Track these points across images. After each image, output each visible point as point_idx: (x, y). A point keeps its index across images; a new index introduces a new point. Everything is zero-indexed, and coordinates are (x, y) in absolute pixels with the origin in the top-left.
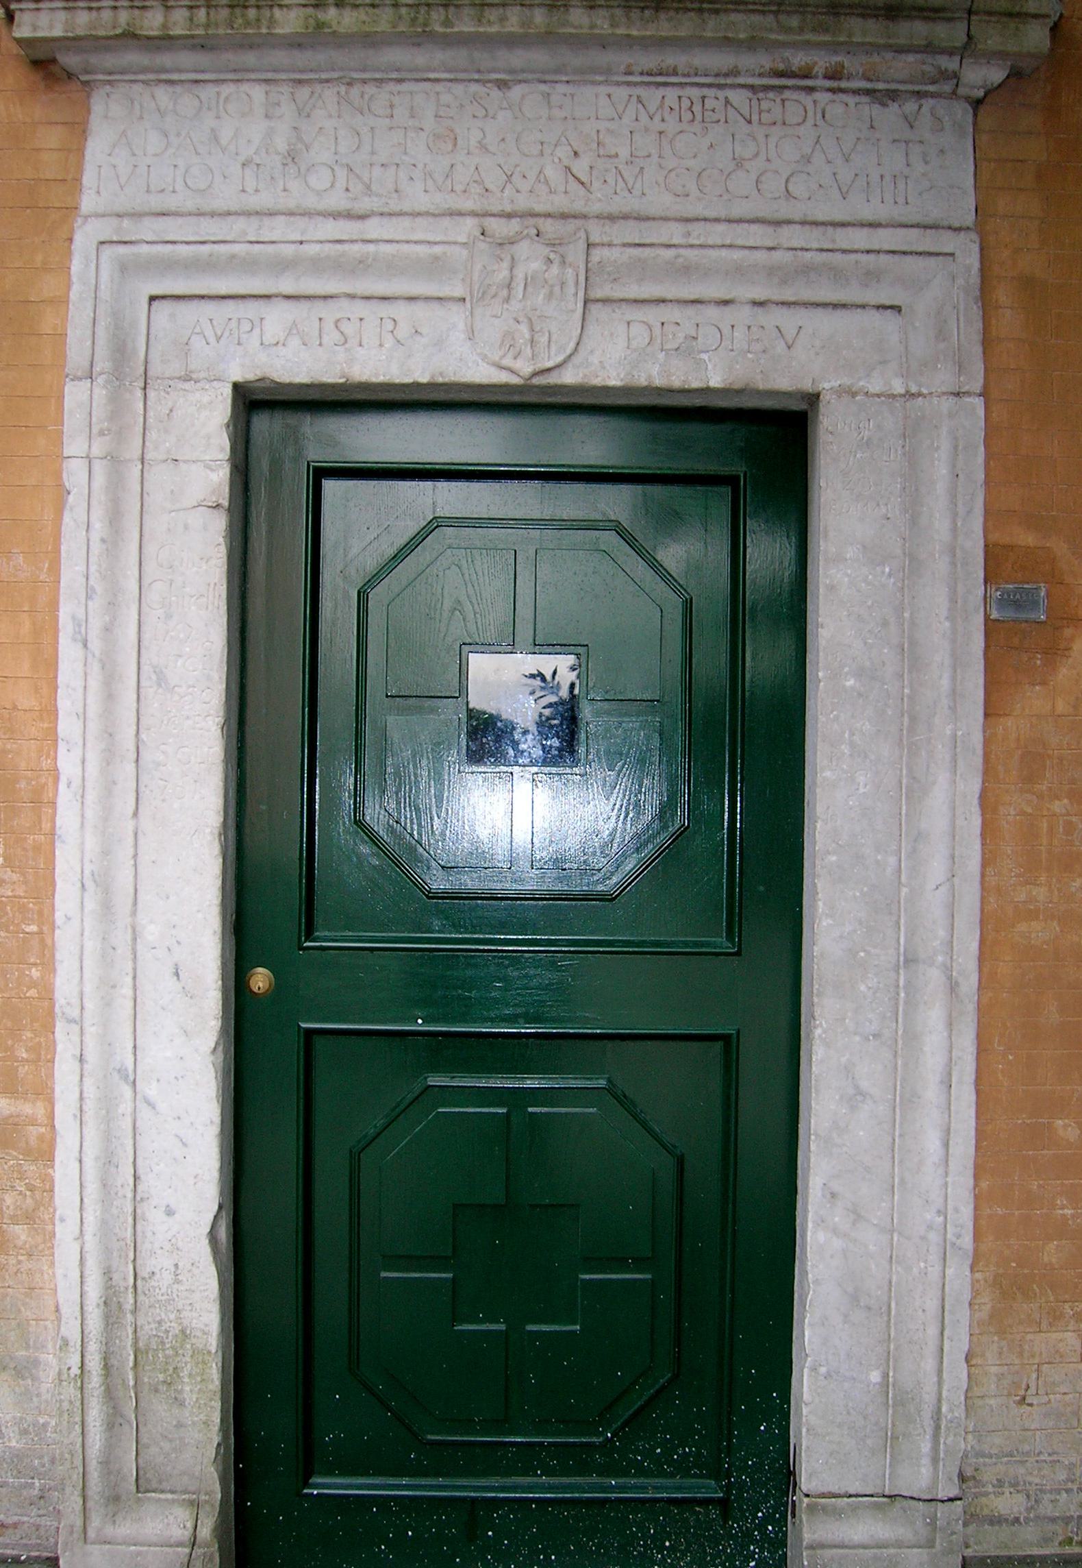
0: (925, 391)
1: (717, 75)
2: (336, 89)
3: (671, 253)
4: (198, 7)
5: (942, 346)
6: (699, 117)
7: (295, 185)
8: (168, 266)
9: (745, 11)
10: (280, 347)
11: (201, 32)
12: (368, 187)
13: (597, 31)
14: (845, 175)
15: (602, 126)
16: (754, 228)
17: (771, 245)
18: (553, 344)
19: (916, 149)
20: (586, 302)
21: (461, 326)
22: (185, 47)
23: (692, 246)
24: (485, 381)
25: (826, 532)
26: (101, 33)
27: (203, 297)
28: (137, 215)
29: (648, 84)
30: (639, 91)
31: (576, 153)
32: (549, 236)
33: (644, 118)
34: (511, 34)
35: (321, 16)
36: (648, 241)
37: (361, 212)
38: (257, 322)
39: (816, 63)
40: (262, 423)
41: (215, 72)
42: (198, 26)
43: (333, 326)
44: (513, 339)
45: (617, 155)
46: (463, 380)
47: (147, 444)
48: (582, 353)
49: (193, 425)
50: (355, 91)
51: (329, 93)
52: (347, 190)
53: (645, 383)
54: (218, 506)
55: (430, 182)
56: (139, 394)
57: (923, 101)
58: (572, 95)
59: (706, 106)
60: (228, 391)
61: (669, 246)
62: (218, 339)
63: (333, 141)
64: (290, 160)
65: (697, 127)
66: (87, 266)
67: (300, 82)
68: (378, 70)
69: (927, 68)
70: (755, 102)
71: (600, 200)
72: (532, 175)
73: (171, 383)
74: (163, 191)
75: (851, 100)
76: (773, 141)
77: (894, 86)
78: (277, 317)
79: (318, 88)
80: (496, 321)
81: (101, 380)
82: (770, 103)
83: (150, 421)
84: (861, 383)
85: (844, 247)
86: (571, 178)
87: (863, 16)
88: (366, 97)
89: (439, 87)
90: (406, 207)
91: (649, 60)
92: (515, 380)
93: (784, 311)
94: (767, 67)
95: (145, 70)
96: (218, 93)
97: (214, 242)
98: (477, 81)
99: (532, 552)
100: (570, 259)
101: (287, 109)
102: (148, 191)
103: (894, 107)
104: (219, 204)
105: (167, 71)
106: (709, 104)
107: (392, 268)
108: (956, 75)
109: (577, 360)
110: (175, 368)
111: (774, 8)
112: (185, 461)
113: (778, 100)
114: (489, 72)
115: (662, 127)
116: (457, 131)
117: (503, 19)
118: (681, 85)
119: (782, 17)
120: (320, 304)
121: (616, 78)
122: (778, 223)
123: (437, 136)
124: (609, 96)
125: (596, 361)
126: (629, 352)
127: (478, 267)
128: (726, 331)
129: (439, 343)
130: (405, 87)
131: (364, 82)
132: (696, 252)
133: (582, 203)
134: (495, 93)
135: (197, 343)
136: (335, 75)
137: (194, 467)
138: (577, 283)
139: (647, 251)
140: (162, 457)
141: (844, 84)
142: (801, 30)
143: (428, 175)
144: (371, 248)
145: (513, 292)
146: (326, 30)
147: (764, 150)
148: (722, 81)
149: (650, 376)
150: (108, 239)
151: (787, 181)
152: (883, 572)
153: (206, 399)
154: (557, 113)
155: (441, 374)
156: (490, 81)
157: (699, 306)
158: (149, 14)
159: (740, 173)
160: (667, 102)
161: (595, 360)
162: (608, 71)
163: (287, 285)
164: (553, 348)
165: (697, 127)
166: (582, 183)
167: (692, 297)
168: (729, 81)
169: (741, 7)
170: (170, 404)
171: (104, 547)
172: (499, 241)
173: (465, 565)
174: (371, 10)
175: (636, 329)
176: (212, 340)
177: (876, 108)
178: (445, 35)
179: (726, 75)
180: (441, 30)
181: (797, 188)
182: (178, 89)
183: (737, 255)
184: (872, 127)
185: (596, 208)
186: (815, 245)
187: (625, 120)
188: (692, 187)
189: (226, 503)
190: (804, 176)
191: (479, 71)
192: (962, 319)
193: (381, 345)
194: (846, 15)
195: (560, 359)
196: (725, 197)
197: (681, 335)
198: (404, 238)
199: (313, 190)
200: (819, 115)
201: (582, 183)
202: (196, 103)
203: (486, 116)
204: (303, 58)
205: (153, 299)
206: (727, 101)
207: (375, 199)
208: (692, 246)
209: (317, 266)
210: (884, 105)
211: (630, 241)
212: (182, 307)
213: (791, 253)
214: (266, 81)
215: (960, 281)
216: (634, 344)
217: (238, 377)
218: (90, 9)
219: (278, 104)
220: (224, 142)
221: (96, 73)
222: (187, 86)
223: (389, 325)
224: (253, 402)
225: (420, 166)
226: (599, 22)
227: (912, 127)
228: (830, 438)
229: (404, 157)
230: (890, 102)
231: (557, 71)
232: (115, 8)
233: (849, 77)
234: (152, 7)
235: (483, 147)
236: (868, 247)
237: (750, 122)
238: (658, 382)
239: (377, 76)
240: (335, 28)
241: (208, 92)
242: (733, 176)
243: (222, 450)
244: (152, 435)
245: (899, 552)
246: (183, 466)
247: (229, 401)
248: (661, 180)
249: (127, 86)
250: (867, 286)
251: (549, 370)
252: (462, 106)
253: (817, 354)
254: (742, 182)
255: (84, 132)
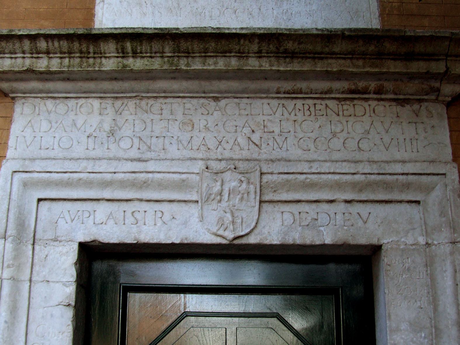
0: (435, 242)
1: (321, 93)
2: (134, 102)
3: (303, 177)
4: (65, 58)
5: (444, 219)
6: (313, 113)
7: (112, 146)
8: (48, 184)
9: (335, 58)
10: (103, 225)
11: (66, 69)
12: (150, 148)
13: (262, 68)
14: (387, 139)
15: (266, 118)
16: (344, 164)
17: (354, 172)
18: (244, 223)
19: (420, 127)
20: (261, 202)
21: (196, 215)
22: (59, 80)
23: (314, 173)
24: (209, 242)
25: (390, 316)
26: (16, 69)
27: (65, 200)
28: (33, 160)
29: (288, 98)
30: (283, 101)
31: (253, 131)
32: (241, 169)
33: (286, 114)
34: (220, 71)
35: (125, 62)
36: (292, 171)
37: (146, 159)
38: (92, 213)
39: (370, 85)
40: (99, 267)
41: (74, 93)
42: (64, 66)
43: (131, 215)
44: (223, 220)
45: (273, 132)
46: (198, 242)
47: (34, 272)
48: (259, 227)
49: (58, 263)
50: (144, 102)
51: (131, 104)
52: (139, 149)
53: (292, 243)
54: (69, 305)
55: (180, 145)
56: (30, 247)
57: (422, 104)
58: (251, 104)
59: (317, 108)
60: (76, 247)
61: (302, 173)
62: (72, 221)
63: (132, 126)
64: (111, 134)
65: (312, 118)
66: (6, 183)
67: (117, 98)
68: (154, 92)
69: (424, 86)
70: (340, 106)
71: (266, 153)
72: (231, 142)
73: (47, 242)
74: (48, 148)
75: (387, 104)
76: (350, 124)
77: (407, 97)
78: (102, 210)
79: (126, 101)
80: (215, 212)
81: (10, 240)
82: (348, 107)
83: (36, 261)
84: (403, 240)
85: (390, 172)
86: (251, 143)
87: (395, 60)
88: (149, 105)
89: (185, 100)
90: (169, 156)
91: (287, 86)
92: (224, 242)
93: (361, 205)
94: (346, 88)
95: (41, 92)
96: (77, 103)
97: (71, 172)
98: (204, 97)
99: (234, 329)
100: (252, 181)
101: (110, 111)
102: (40, 149)
103: (408, 107)
104: (75, 155)
105: (51, 92)
106: (318, 107)
107: (161, 186)
108: (438, 90)
109: (256, 231)
110: (50, 235)
111: (351, 56)
112: (53, 282)
113: (351, 105)
114: (210, 93)
115: (295, 118)
116: (194, 121)
117: (216, 63)
118: (304, 98)
119: (354, 61)
120: (125, 203)
121: (271, 95)
122: (356, 162)
123: (184, 124)
124: (269, 104)
125: (266, 232)
126: (283, 227)
127: (205, 185)
128: (332, 216)
129: (185, 223)
130: (168, 100)
131: (148, 98)
132: (316, 176)
133: (257, 154)
134: (213, 103)
135: (61, 222)
136: (134, 95)
137: (57, 285)
138: (256, 192)
139: (291, 177)
140: (41, 280)
141: (383, 96)
142: (364, 67)
143: (179, 141)
144: (150, 175)
145: (223, 198)
146: (128, 69)
147: (346, 128)
148: (324, 96)
149: (294, 239)
150: (17, 170)
151: (358, 143)
152: (421, 336)
153: (65, 250)
154: (243, 112)
155: (186, 239)
156: (209, 97)
157: (318, 204)
158: (41, 61)
159: (335, 139)
160: (298, 107)
161: (265, 231)
162: (267, 91)
163: (107, 194)
164: (244, 225)
165: (312, 118)
166: (257, 145)
167: (314, 199)
168: (327, 96)
169: (334, 56)
170: (46, 253)
171: (6, 325)
172: (215, 172)
173: (200, 336)
174: (150, 59)
175: (286, 216)
176: (69, 221)
177: (399, 108)
178: (187, 71)
179: (326, 93)
180: (185, 68)
181: (364, 145)
182: (58, 101)
183: (337, 177)
184: (398, 116)
185: (264, 156)
186: (376, 172)
187: (277, 115)
188: (312, 146)
189: (73, 304)
190: (367, 140)
191: (204, 93)
192: (452, 205)
193: (155, 225)
194: (386, 59)
195: (248, 230)
196: (328, 150)
197: (310, 218)
198: (167, 171)
199: (122, 149)
200: (372, 112)
201: (257, 145)
202: (66, 108)
203: (208, 114)
204: (117, 85)
205: (40, 200)
206: (327, 106)
207: (153, 153)
208: (314, 173)
209: (123, 185)
210: (403, 106)
211: (282, 171)
212: (54, 204)
213: (364, 176)
214: (101, 98)
215: (449, 188)
216: (286, 223)
217: (82, 240)
218: (11, 58)
219: (106, 108)
220: (79, 126)
221: (17, 93)
222: (62, 100)
223: (159, 215)
224: (91, 254)
225: (176, 138)
226: (264, 64)
227: (417, 116)
228: (389, 268)
229: (167, 133)
230: (406, 105)
231: (243, 92)
232: (24, 58)
233: (386, 92)
234: (42, 57)
235: (207, 128)
236: (402, 172)
237: (338, 115)
238: (298, 242)
239: (155, 95)
240: (132, 68)
241: (72, 103)
242: (332, 141)
243: (73, 276)
244: (36, 268)
245: (428, 325)
246: (52, 284)
247: (77, 252)
248: (296, 143)
249: (33, 99)
250: (402, 191)
251: (242, 236)
252: (196, 109)
253: (379, 226)
254: (337, 143)
255: (11, 121)
